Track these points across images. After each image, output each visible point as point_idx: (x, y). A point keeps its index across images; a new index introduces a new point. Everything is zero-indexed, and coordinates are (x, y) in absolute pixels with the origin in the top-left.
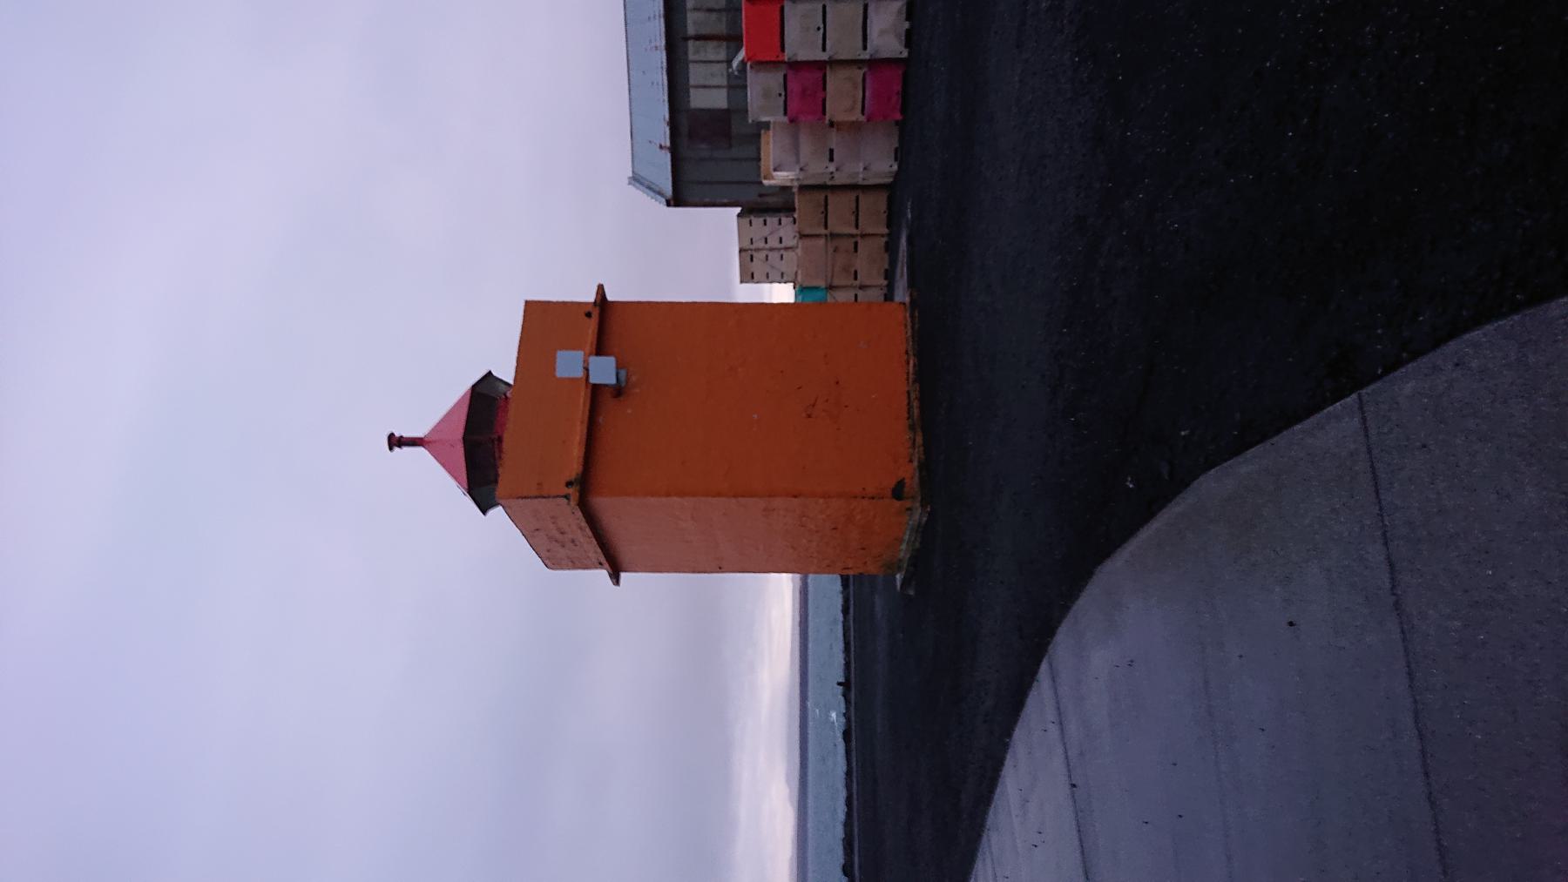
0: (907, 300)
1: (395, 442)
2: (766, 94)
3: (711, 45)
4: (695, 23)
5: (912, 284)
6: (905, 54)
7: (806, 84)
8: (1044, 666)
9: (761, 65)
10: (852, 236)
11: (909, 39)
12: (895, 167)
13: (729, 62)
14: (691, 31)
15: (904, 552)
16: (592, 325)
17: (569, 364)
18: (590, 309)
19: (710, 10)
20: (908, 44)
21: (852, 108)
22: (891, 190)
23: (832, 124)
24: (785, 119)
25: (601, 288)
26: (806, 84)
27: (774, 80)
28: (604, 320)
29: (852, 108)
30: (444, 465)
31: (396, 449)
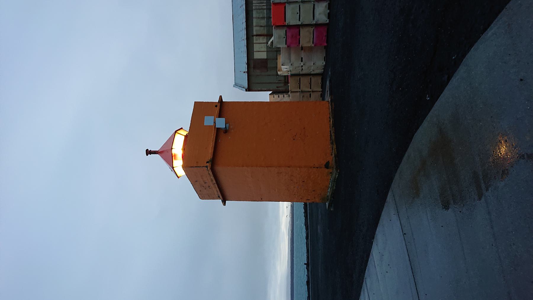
0: (330, 100)
1: (148, 152)
2: (279, 37)
3: (261, 37)
4: (256, 31)
5: (331, 94)
6: (328, 22)
7: (293, 32)
8: (390, 193)
9: (278, 27)
10: (309, 92)
11: (329, 16)
12: (324, 63)
13: (267, 43)
14: (255, 33)
15: (329, 192)
16: (218, 109)
17: (209, 121)
18: (217, 104)
19: (261, 26)
20: (329, 17)
21: (309, 42)
22: (323, 76)
23: (302, 48)
24: (286, 46)
25: (221, 97)
26: (293, 32)
27: (282, 32)
28: (221, 107)
29: (309, 42)
30: (164, 159)
31: (149, 155)
